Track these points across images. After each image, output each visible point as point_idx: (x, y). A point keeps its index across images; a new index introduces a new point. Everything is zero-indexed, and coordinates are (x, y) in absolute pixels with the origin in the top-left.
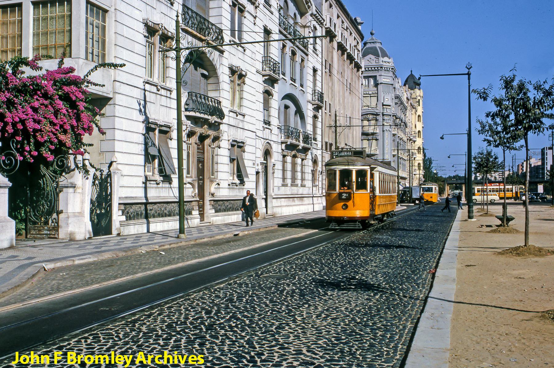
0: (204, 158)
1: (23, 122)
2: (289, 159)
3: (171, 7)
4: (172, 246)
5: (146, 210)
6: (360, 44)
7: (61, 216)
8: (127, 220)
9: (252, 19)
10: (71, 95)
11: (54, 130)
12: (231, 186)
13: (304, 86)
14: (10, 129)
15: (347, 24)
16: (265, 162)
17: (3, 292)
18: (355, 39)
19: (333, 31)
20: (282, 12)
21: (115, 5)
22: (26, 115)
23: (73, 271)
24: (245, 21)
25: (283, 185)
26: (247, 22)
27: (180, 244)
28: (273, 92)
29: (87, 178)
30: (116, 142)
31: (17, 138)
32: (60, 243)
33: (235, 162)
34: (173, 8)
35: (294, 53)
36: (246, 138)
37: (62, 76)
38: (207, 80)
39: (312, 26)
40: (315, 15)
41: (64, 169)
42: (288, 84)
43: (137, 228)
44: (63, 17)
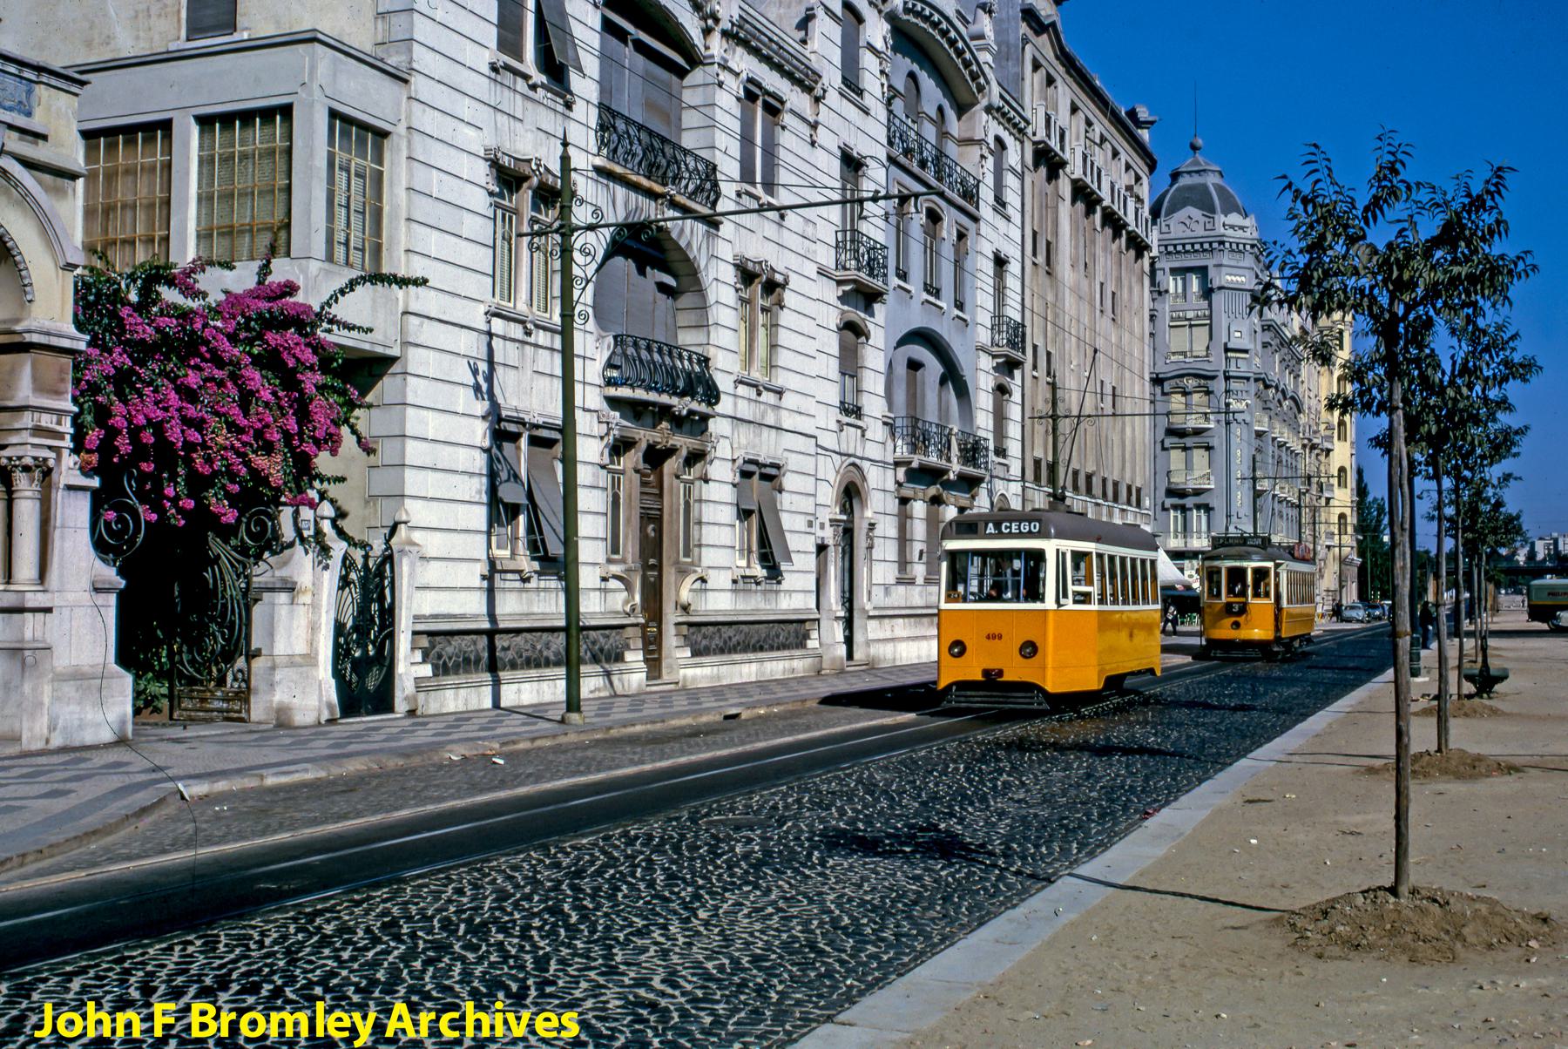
0: (661, 510)
1: (158, 428)
2: (919, 508)
3: (567, 112)
4: (539, 743)
5: (492, 648)
6: (1145, 180)
7: (257, 664)
8: (435, 675)
9: (805, 130)
10: (285, 355)
11: (237, 444)
12: (741, 585)
13: (968, 307)
14: (123, 444)
15: (1101, 126)
16: (844, 517)
17: (51, 846)
18: (1128, 167)
19: (1057, 149)
20: (898, 105)
21: (409, 117)
22: (166, 409)
23: (250, 803)
24: (785, 139)
25: (900, 582)
26: (791, 140)
27: (562, 740)
28: (871, 327)
29: (326, 567)
30: (408, 472)
31: (144, 466)
32: (251, 732)
33: (755, 519)
35: (934, 217)
36: (786, 454)
37: (264, 305)
38: (675, 299)
39: (991, 140)
40: (999, 109)
41: (268, 542)
42: (916, 304)
43: (466, 696)
44: (271, 152)
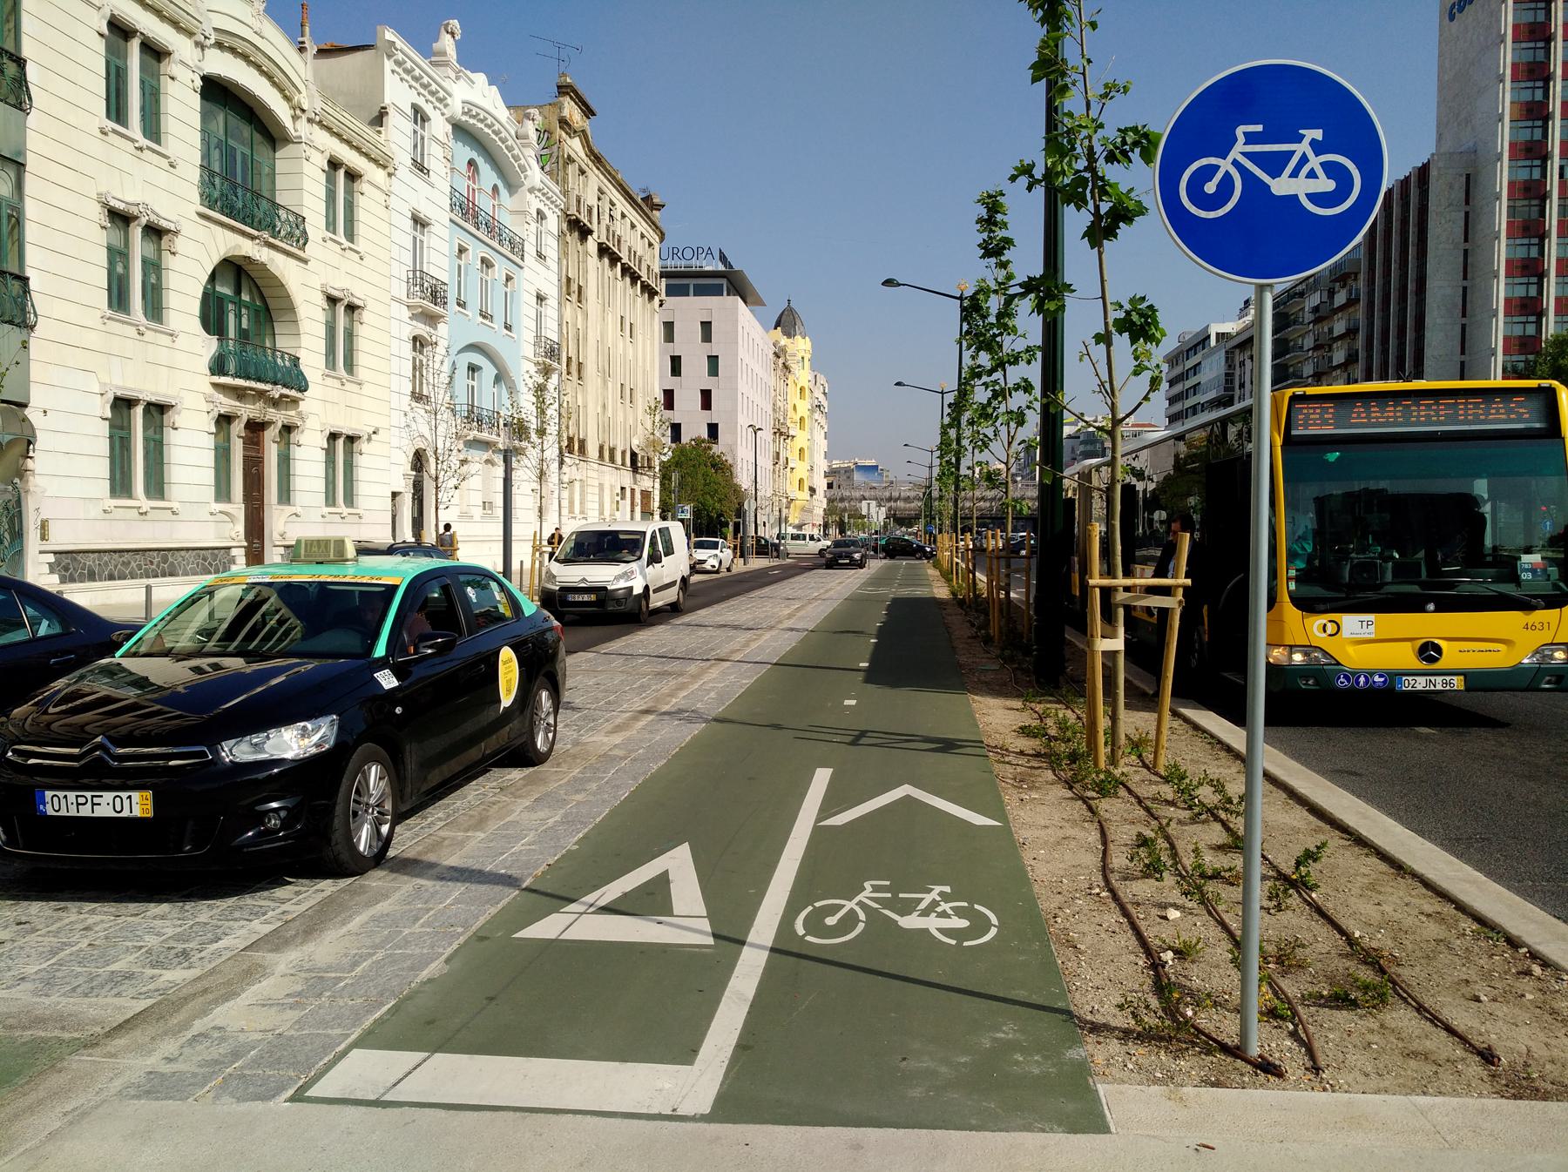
13: (134, 210)
18: (643, 236)
34: (176, 345)
